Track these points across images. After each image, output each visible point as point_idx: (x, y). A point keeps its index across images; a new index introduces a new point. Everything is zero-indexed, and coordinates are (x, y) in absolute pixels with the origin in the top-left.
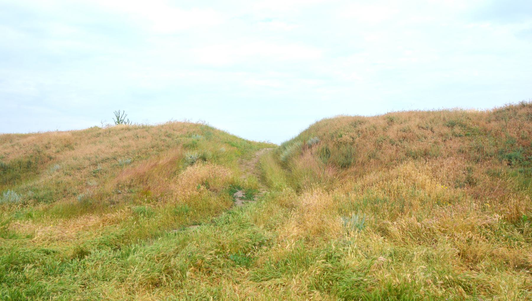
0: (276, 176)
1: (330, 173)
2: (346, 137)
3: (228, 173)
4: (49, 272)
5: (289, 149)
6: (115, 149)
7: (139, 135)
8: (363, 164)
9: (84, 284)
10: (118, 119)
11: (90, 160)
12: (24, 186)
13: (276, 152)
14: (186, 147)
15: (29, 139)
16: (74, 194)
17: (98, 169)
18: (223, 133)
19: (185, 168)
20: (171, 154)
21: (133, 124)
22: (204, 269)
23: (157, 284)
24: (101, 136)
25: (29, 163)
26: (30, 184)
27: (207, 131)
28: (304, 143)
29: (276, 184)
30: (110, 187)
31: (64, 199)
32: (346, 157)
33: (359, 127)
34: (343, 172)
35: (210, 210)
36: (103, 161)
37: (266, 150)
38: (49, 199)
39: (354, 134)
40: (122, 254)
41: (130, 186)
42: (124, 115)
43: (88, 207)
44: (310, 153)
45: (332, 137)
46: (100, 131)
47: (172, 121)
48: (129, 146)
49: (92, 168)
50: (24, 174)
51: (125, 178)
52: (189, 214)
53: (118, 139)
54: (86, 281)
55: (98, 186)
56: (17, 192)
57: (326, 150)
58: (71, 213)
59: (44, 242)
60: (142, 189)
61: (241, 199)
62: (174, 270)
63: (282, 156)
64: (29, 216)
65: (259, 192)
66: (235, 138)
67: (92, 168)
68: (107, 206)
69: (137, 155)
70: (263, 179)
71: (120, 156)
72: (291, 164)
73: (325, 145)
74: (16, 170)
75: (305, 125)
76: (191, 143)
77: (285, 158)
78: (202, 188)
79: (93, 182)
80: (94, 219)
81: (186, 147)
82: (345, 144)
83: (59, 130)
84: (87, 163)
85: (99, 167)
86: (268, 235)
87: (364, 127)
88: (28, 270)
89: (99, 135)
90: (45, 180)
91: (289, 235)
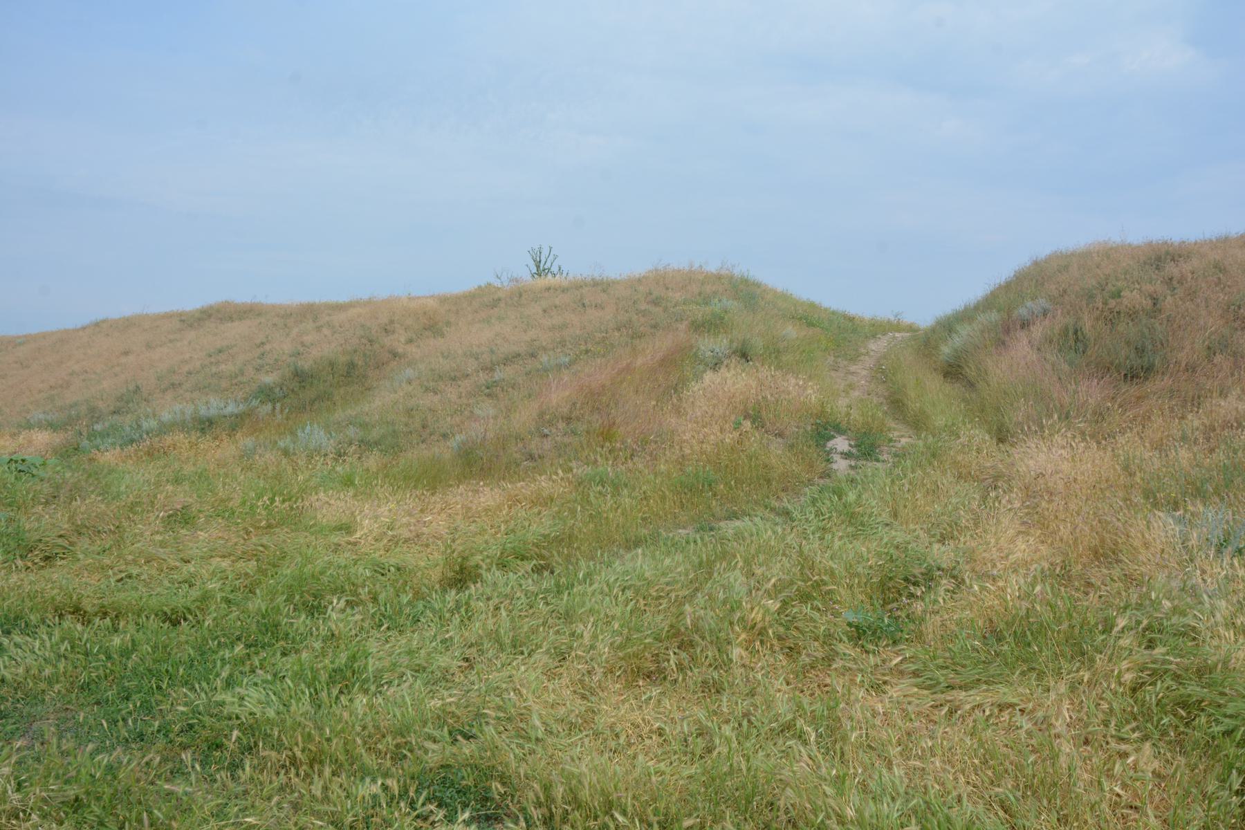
0: (934, 396)
1: (1092, 393)
2: (1133, 298)
3: (801, 391)
4: (390, 620)
5: (964, 332)
6: (532, 334)
7: (586, 302)
8: (1191, 368)
9: (467, 660)
10: (538, 267)
11: (477, 359)
12: (339, 415)
13: (926, 342)
14: (699, 327)
15: (353, 312)
16: (445, 436)
17: (497, 378)
18: (785, 297)
19: (698, 377)
20: (661, 344)
21: (571, 276)
22: (775, 642)
23: (655, 675)
24: (502, 305)
25: (352, 365)
26: (350, 412)
27: (747, 293)
28: (1006, 312)
29: (940, 421)
30: (524, 417)
31: (424, 446)
32: (1140, 351)
33: (1171, 269)
34: (1131, 390)
35: (769, 481)
36: (508, 360)
37: (894, 338)
38: (391, 444)
39: (1159, 287)
40: (557, 585)
41: (568, 420)
42: (551, 257)
43: (476, 464)
44: (1025, 341)
45: (1091, 297)
46: (500, 294)
47: (660, 267)
48: (564, 326)
49: (483, 377)
50: (342, 391)
51: (558, 396)
52: (713, 492)
53: (541, 312)
54: (474, 650)
55: (495, 418)
56: (327, 428)
57: (1076, 332)
58: (431, 479)
59: (377, 545)
60: (595, 426)
61: (846, 456)
62: (697, 638)
63: (946, 350)
64: (348, 482)
65: (890, 440)
66: (813, 306)
67: (483, 377)
68: (518, 465)
69: (583, 347)
70: (897, 404)
71: (545, 349)
72: (970, 372)
73: (1070, 320)
74: (325, 381)
75: (1004, 271)
76: (702, 320)
77: (953, 356)
78: (747, 425)
79: (486, 409)
80: (488, 496)
81: (699, 327)
82: (1133, 315)
83: (413, 295)
84: (471, 365)
85: (498, 375)
86: (942, 554)
87: (1186, 267)
88: (336, 615)
89: (495, 303)
90: (383, 401)
91: (1009, 560)
